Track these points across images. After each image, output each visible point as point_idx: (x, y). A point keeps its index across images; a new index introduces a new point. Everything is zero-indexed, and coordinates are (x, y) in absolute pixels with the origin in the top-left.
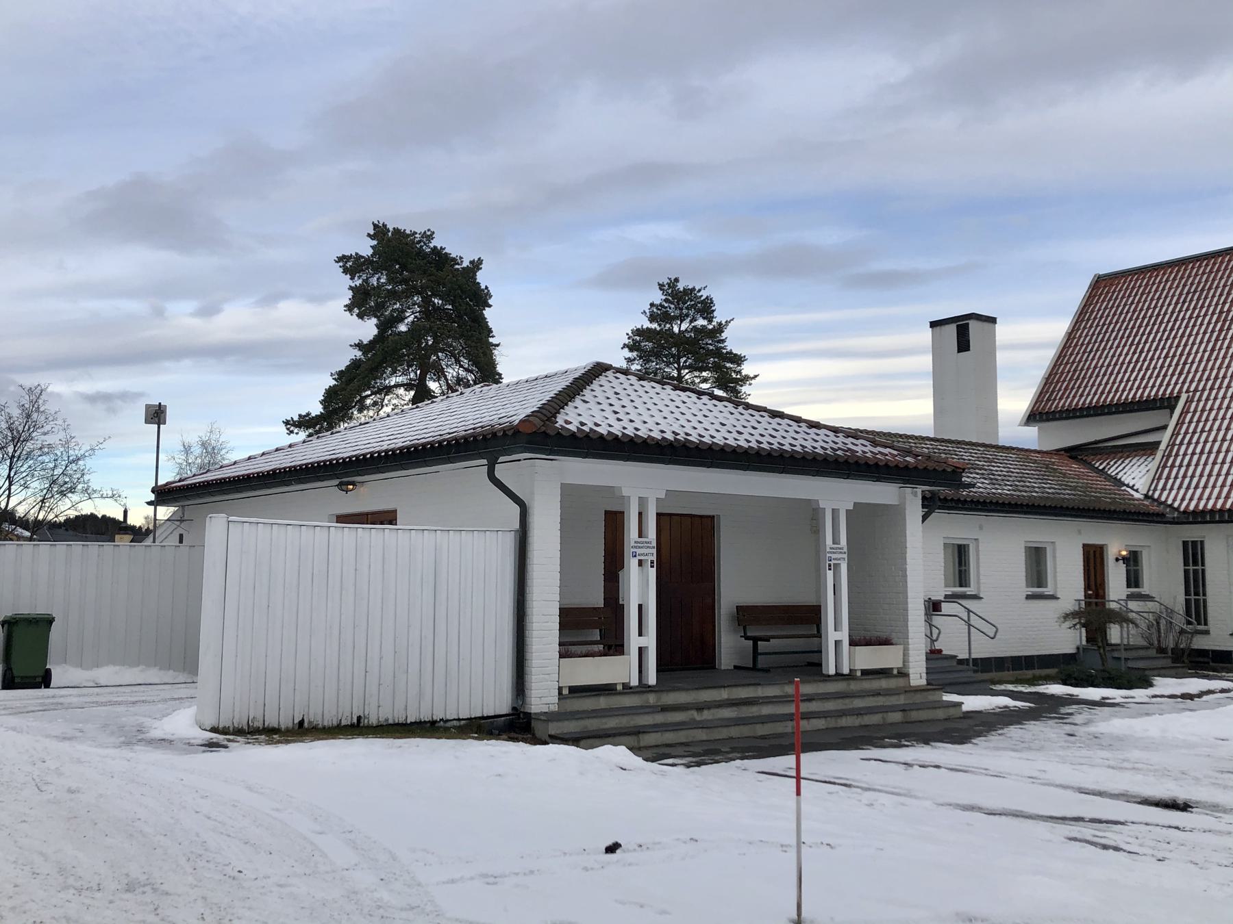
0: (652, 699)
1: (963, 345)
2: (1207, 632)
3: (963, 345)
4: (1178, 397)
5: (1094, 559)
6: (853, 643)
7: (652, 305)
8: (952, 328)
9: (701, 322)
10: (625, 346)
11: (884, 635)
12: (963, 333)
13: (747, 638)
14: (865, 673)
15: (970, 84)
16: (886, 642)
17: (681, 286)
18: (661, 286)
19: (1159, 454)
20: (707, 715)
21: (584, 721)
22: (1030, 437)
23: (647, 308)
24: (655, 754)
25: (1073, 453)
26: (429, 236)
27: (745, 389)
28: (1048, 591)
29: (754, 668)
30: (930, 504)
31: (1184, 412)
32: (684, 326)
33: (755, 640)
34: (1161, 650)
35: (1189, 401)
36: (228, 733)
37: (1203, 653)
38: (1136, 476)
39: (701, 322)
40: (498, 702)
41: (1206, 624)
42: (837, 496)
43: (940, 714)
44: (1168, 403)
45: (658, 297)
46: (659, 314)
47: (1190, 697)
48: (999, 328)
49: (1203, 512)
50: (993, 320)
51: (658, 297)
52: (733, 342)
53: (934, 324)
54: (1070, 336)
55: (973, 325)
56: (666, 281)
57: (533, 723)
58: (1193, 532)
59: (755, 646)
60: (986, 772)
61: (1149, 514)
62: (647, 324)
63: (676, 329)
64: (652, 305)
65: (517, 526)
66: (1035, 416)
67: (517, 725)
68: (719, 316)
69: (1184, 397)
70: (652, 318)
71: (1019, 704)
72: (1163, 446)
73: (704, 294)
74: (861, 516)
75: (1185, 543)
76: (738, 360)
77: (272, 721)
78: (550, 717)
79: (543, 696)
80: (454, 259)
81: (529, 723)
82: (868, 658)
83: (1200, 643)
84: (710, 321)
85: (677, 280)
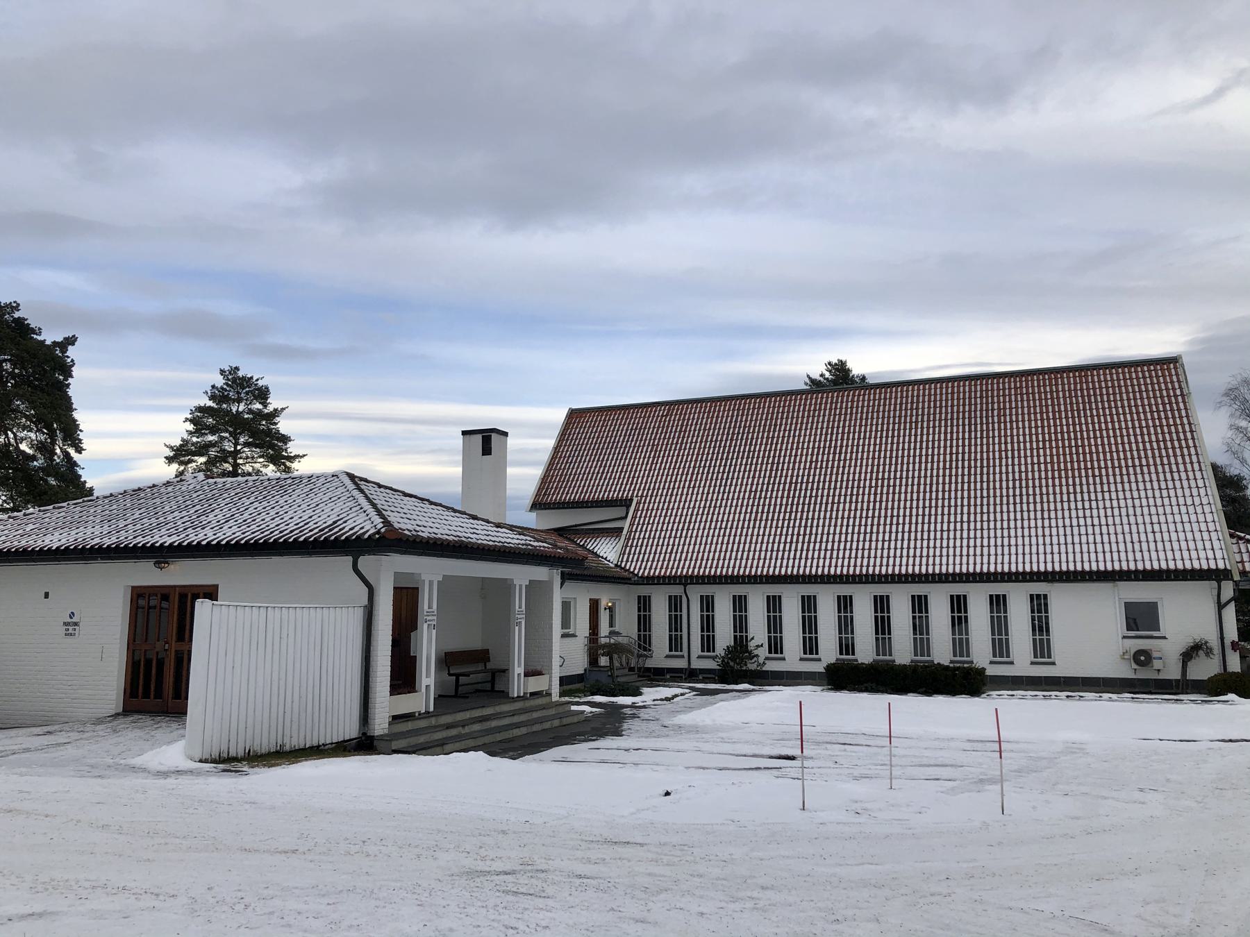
0: (433, 721)
1: (487, 450)
2: (784, 659)
3: (487, 450)
4: (631, 500)
5: (594, 606)
6: (526, 675)
7: (213, 387)
8: (479, 437)
9: (258, 406)
10: (187, 420)
11: (539, 668)
12: (486, 441)
13: (450, 675)
14: (532, 694)
15: (356, 202)
16: (540, 673)
17: (240, 374)
18: (222, 372)
19: (623, 538)
20: (467, 730)
21: (411, 738)
22: (531, 520)
23: (209, 389)
24: (492, 754)
25: (561, 532)
26: (17, 307)
27: (295, 465)
28: (571, 631)
29: (456, 696)
30: (565, 578)
31: (636, 510)
32: (242, 408)
33: (457, 676)
34: (631, 669)
35: (638, 503)
36: (228, 761)
37: (649, 669)
38: (608, 551)
39: (258, 406)
40: (350, 729)
41: (968, 655)
42: (521, 575)
43: (575, 719)
44: (626, 503)
45: (220, 381)
46: (219, 396)
47: (58, 745)
48: (510, 441)
49: (653, 577)
50: (506, 434)
51: (220, 381)
52: (284, 425)
53: (464, 433)
54: (556, 449)
55: (494, 435)
56: (227, 368)
57: (375, 743)
58: (644, 590)
59: (457, 680)
60: (667, 749)
61: (618, 577)
62: (210, 404)
63: (234, 409)
64: (213, 387)
65: (365, 602)
66: (537, 505)
67: (365, 744)
68: (274, 403)
69: (635, 500)
70: (212, 398)
71: (594, 710)
72: (625, 532)
73: (260, 383)
74: (533, 586)
75: (639, 597)
76: (285, 439)
77: (233, 753)
78: (381, 738)
79: (380, 725)
80: (33, 331)
81: (372, 743)
82: (535, 684)
83: (650, 663)
84: (265, 407)
85: (237, 369)
